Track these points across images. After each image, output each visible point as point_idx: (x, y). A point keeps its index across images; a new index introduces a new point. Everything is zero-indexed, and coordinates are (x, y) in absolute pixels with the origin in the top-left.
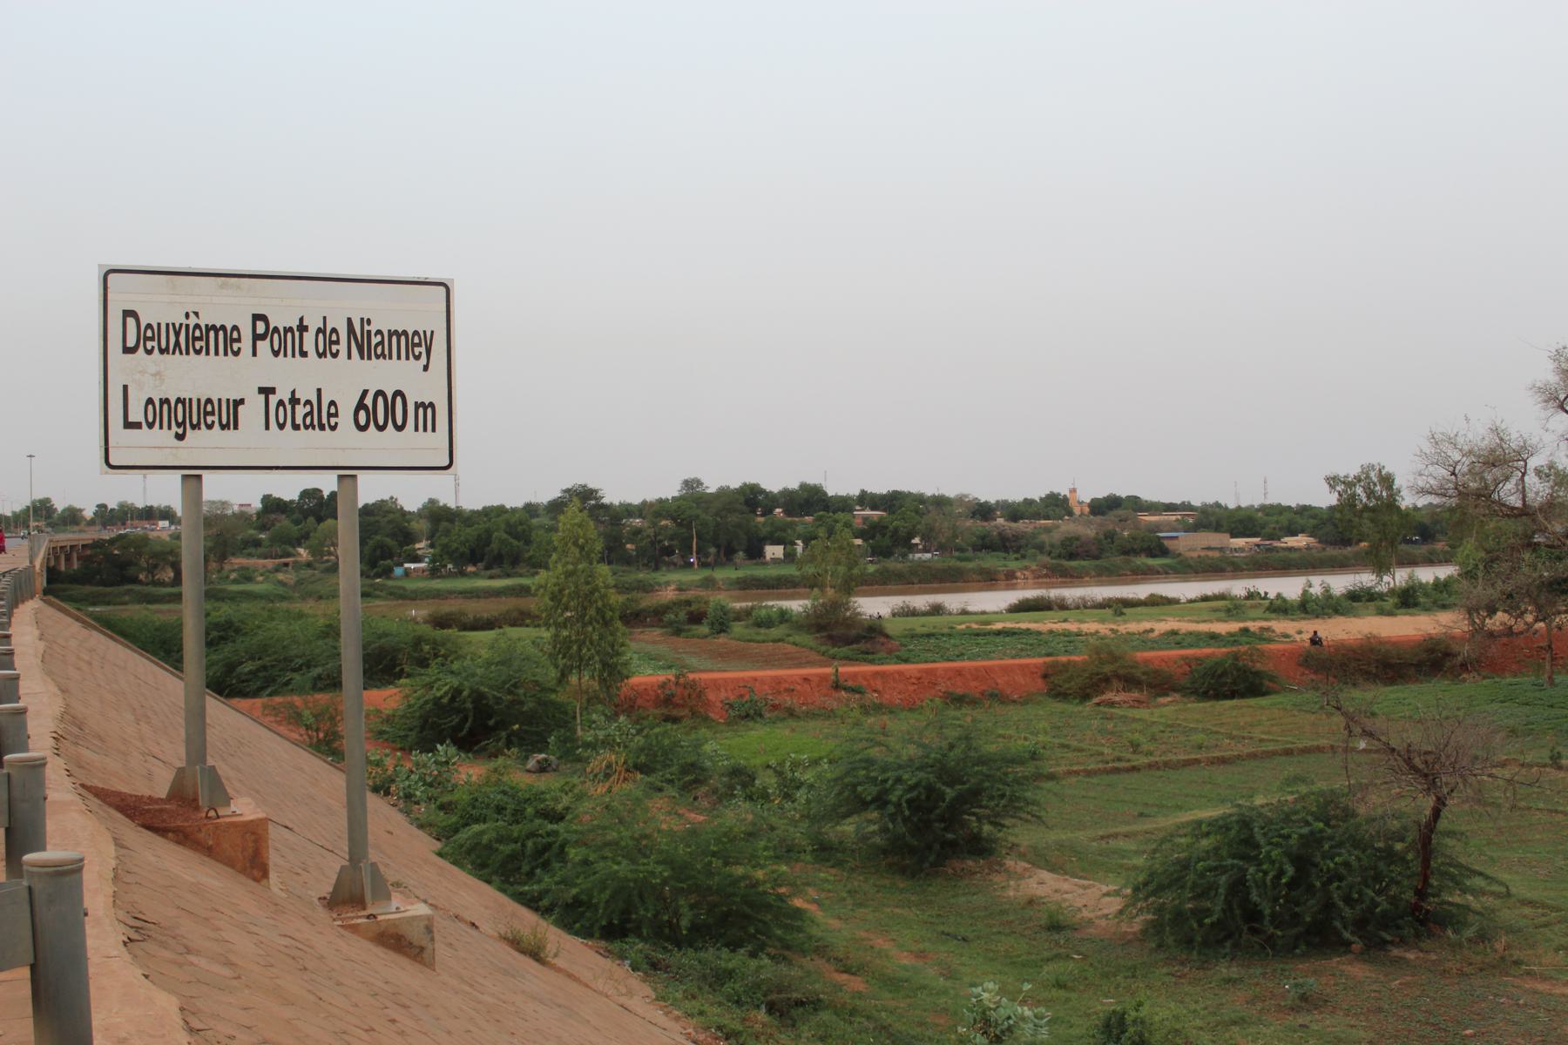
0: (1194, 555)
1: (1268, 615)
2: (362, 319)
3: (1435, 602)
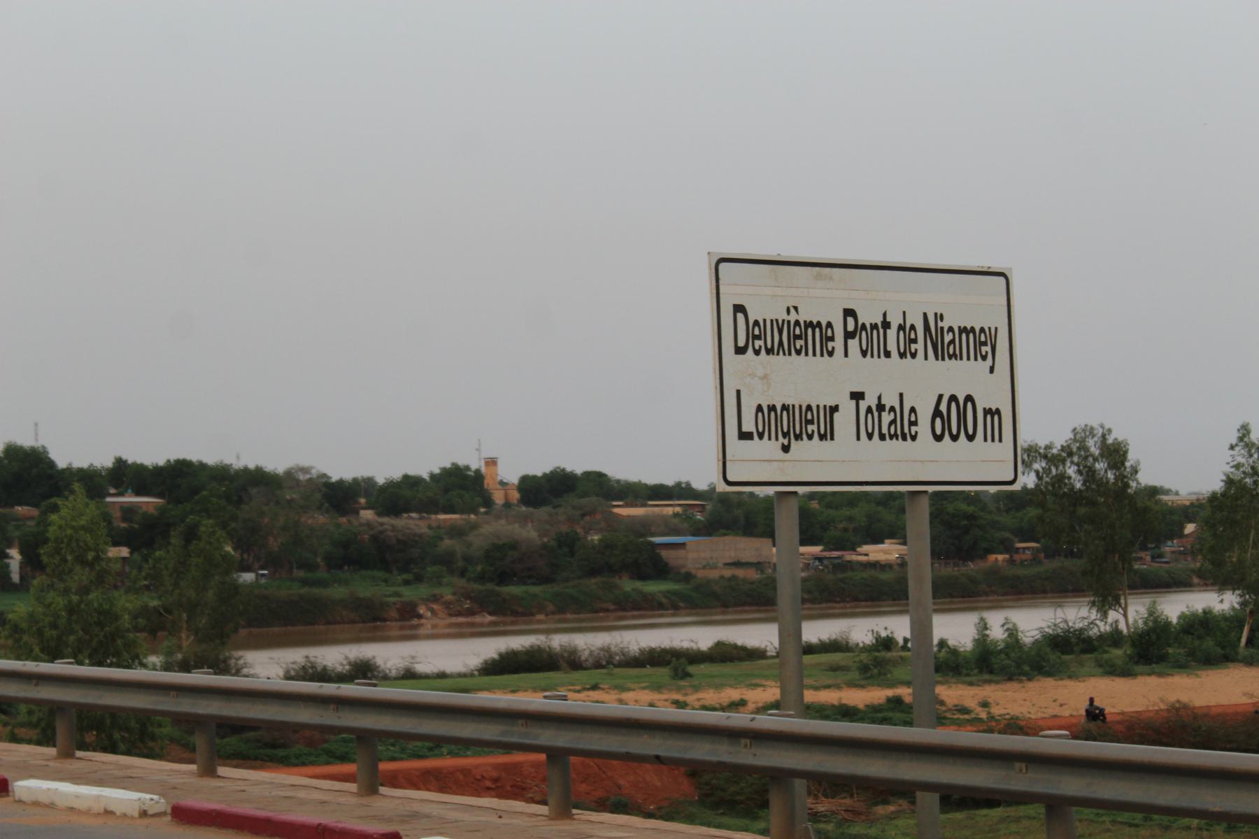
0: (713, 574)
2: (936, 314)
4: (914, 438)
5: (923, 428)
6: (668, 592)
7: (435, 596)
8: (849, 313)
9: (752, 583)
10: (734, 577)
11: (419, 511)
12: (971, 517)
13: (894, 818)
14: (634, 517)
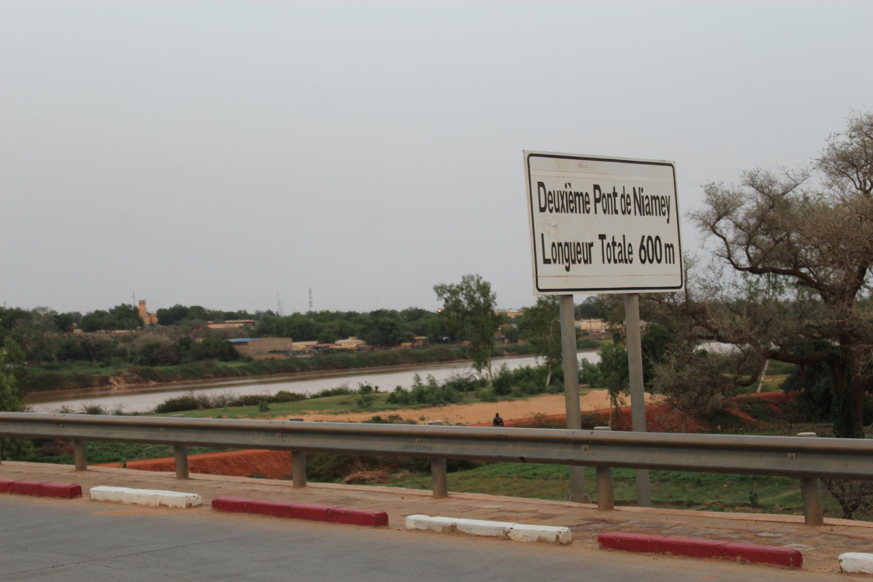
0: (263, 357)
1: (389, 405)
2: (639, 188)
3: (523, 390)
4: (631, 262)
5: (635, 256)
6: (241, 367)
7: (118, 373)
8: (596, 187)
9: (284, 361)
10: (273, 359)
11: (105, 328)
12: (392, 325)
13: (404, 480)
14: (220, 329)
